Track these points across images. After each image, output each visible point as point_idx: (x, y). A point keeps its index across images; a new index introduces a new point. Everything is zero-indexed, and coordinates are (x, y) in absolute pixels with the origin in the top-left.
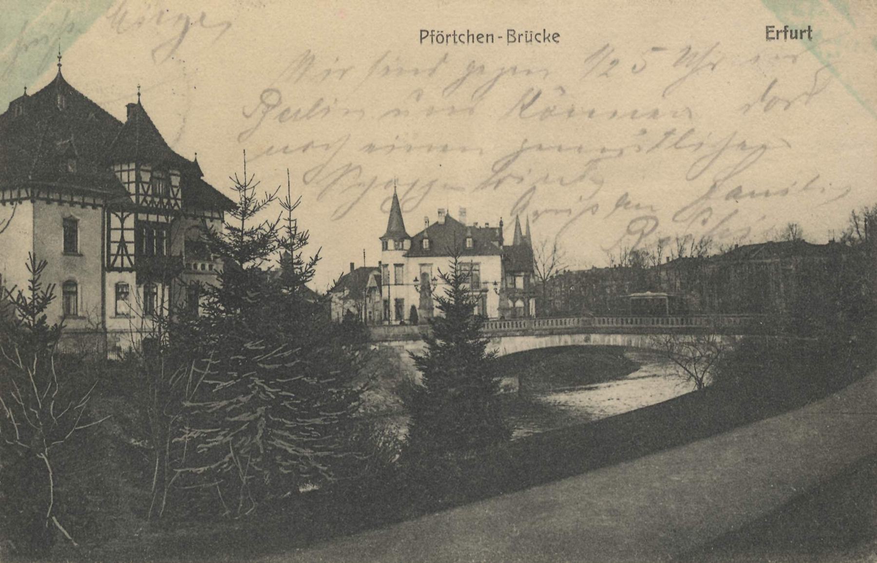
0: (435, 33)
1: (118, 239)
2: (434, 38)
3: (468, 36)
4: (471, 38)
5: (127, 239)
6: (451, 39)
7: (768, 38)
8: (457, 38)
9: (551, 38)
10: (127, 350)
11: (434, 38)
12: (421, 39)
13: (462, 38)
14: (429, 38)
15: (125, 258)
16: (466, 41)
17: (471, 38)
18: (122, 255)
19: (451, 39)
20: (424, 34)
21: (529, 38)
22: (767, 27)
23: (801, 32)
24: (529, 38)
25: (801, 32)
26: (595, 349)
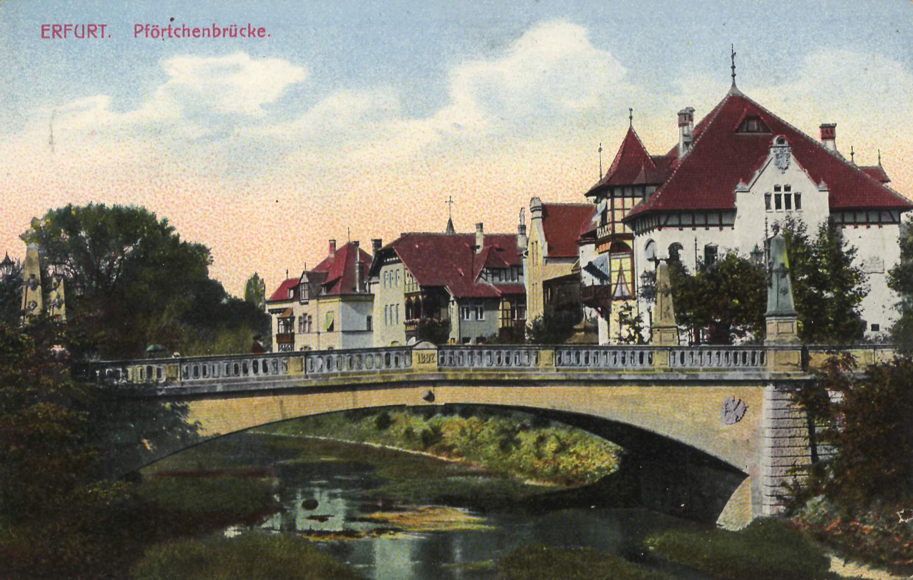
0: (150, 28)
1: (618, 268)
2: (149, 32)
3: (184, 30)
4: (186, 32)
5: (624, 268)
6: (166, 33)
7: (43, 36)
8: (172, 32)
9: (256, 33)
10: (893, 360)
11: (149, 32)
12: (136, 33)
13: (243, 32)
14: (144, 31)
15: (624, 286)
16: (63, 36)
17: (186, 32)
18: (622, 284)
19: (166, 33)
20: (138, 28)
21: (233, 33)
22: (43, 26)
23: (163, 30)
24: (233, 33)
25: (163, 30)
26: (354, 271)
